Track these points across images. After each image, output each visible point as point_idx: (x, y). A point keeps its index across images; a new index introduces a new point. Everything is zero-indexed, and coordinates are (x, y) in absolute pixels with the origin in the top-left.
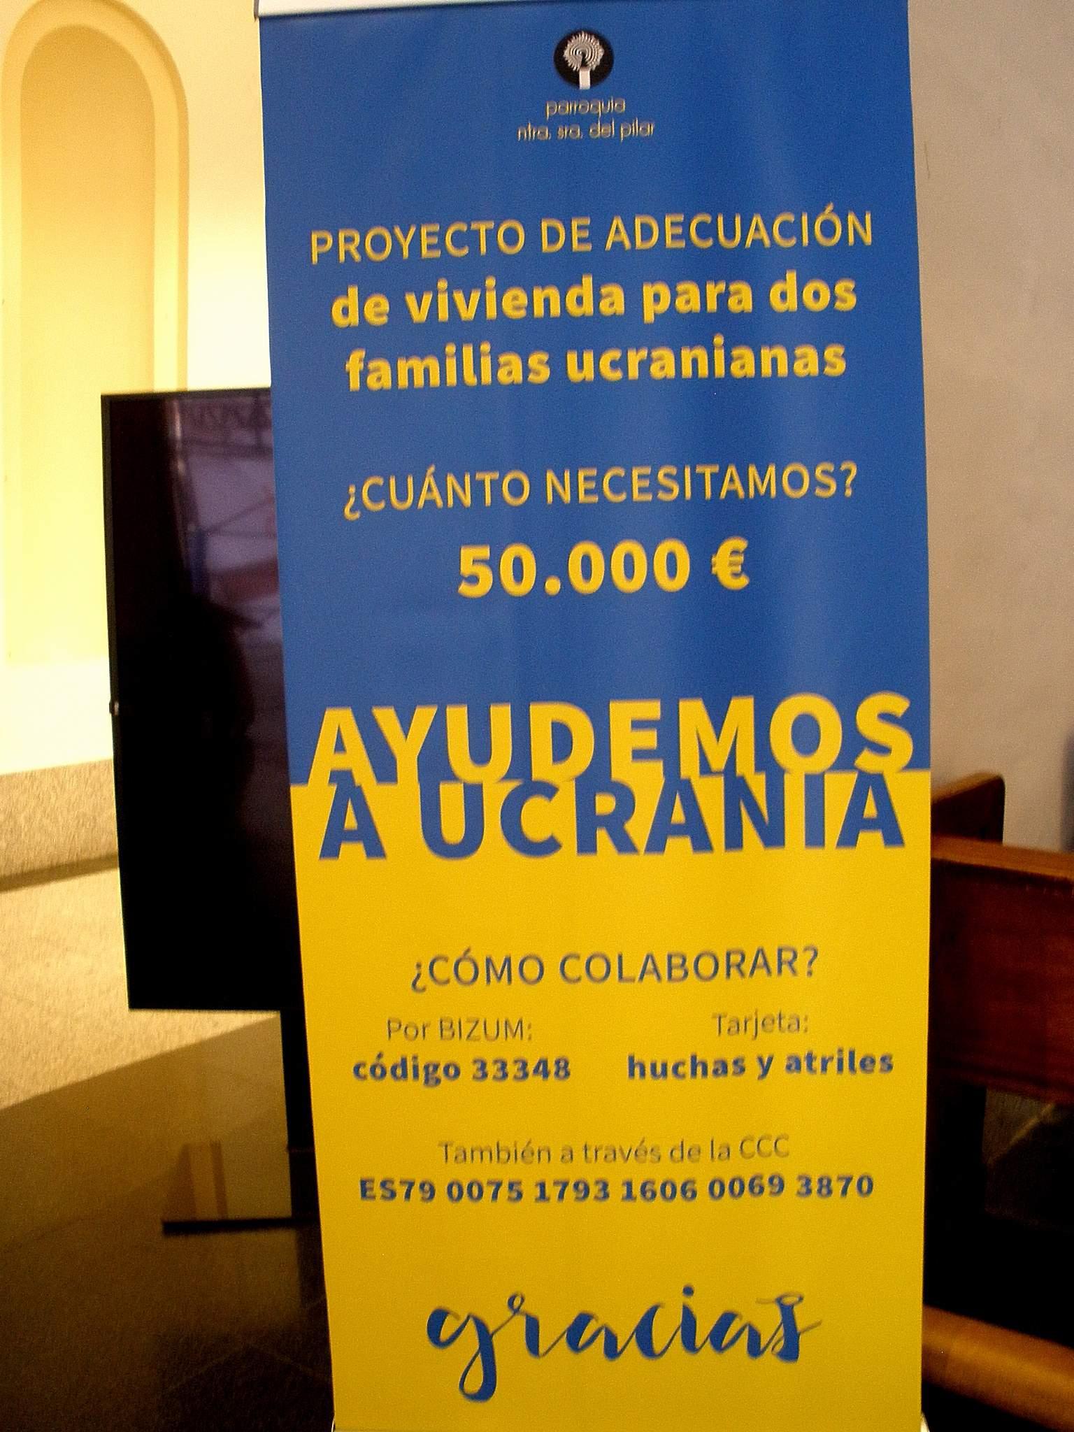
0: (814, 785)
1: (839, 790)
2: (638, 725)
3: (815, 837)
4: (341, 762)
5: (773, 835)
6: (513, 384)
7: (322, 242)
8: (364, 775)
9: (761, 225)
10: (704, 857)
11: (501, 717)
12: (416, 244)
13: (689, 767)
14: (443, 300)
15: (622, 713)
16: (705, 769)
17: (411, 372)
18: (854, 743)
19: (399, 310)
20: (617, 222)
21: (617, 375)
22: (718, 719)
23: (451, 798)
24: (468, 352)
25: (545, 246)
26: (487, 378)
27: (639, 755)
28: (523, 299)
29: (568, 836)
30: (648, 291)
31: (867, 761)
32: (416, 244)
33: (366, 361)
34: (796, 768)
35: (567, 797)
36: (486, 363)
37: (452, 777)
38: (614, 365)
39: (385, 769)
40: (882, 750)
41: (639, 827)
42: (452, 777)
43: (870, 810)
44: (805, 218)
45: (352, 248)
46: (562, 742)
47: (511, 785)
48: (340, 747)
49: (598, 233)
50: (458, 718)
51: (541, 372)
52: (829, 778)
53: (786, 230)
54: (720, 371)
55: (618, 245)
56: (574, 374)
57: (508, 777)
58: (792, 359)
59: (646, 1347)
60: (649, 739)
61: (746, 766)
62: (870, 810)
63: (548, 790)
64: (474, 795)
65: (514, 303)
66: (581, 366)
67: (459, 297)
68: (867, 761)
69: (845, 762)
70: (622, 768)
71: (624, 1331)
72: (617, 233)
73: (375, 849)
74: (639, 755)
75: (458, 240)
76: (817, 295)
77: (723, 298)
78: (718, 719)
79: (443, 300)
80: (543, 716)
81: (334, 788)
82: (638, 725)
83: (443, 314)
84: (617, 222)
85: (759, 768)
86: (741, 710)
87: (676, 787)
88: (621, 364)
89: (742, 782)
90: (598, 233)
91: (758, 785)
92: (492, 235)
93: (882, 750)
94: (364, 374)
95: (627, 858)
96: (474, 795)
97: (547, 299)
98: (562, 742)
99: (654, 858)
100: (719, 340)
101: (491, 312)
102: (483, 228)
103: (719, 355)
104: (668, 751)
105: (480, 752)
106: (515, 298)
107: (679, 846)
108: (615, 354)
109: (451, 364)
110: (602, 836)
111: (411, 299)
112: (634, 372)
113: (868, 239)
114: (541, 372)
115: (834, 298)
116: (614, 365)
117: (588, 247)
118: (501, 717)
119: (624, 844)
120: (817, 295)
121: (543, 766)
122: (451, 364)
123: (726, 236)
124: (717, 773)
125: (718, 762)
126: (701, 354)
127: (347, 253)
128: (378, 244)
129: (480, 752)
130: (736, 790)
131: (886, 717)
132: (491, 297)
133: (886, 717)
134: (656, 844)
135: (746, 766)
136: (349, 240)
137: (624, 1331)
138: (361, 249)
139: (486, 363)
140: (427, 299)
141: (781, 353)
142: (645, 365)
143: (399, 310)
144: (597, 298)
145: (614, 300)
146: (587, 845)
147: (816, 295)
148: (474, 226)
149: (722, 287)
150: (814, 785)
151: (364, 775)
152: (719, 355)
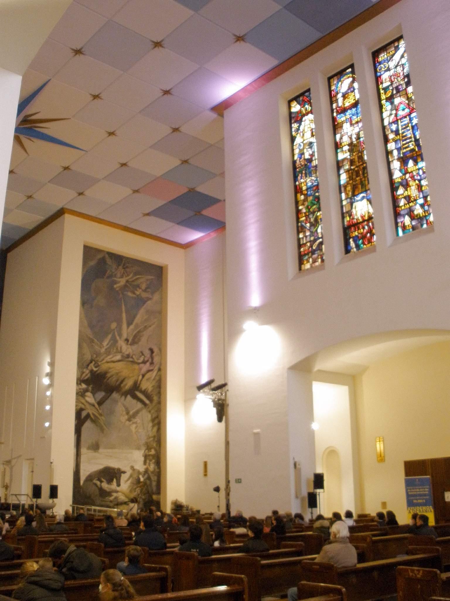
1: (429, 510)
70: (420, 509)
87: (423, 510)
130: (425, 510)
150: (428, 510)
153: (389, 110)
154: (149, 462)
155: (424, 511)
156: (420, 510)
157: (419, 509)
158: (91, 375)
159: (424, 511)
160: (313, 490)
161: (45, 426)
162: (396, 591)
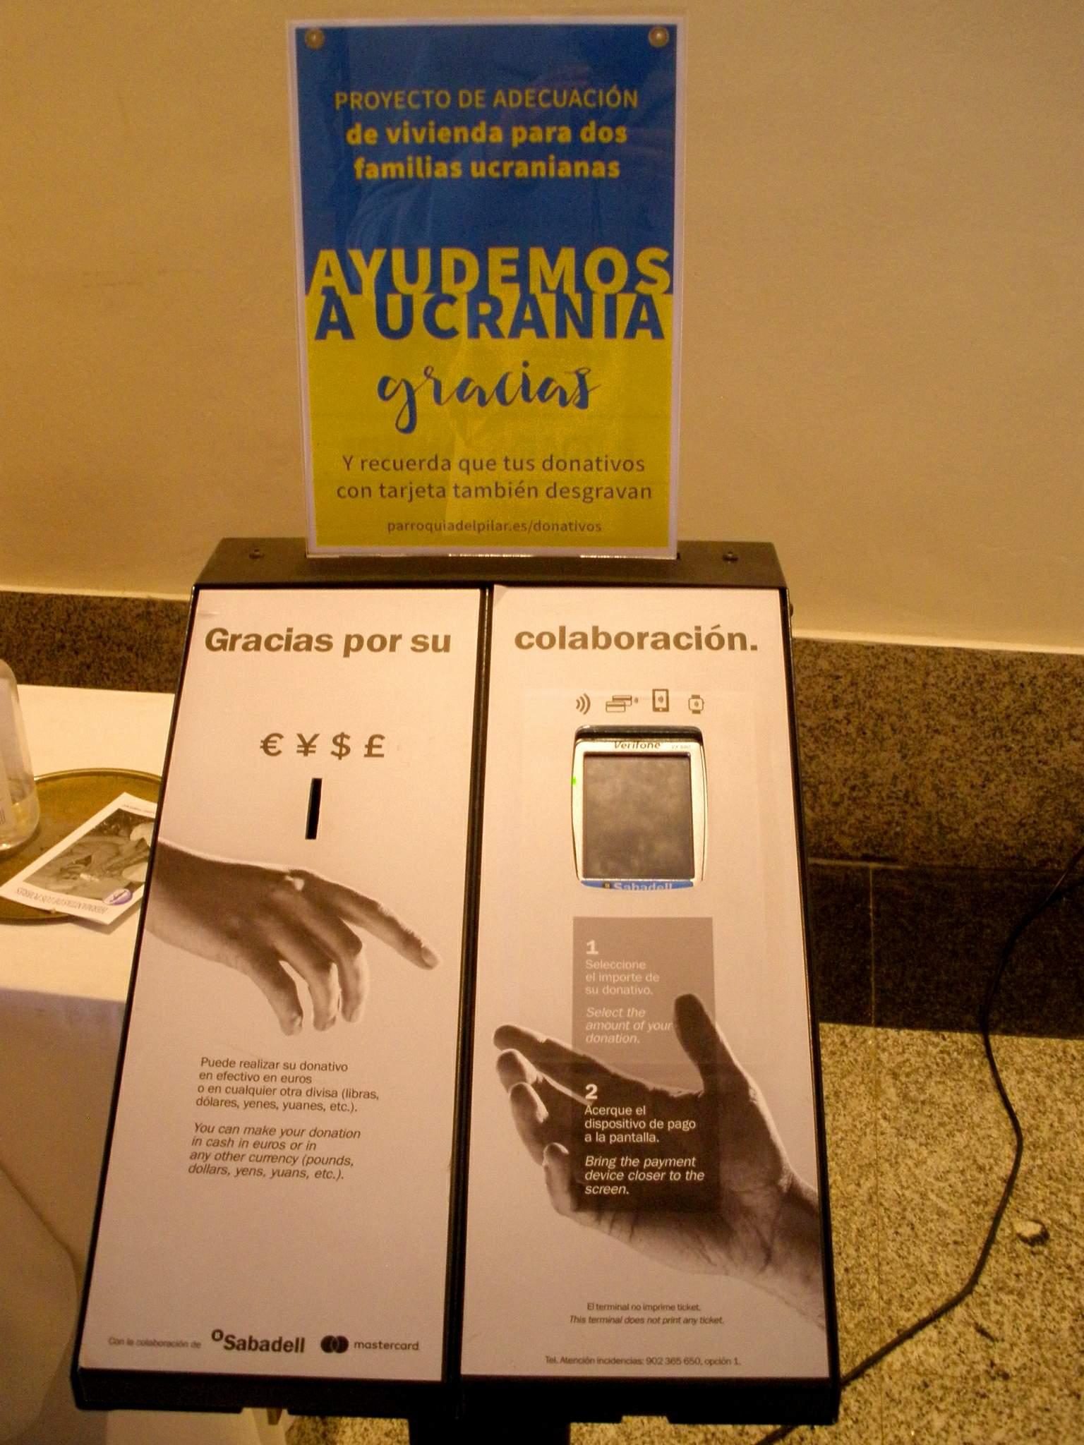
0: (611, 301)
1: (626, 304)
2: (506, 262)
3: (611, 332)
4: (329, 282)
5: (585, 330)
6: (442, 178)
7: (341, 98)
8: (342, 290)
9: (577, 95)
10: (544, 341)
11: (424, 256)
12: (392, 101)
13: (535, 287)
14: (406, 132)
15: (496, 255)
16: (545, 289)
17: (389, 171)
18: (635, 276)
19: (383, 137)
20: (500, 93)
21: (497, 175)
22: (553, 259)
23: (394, 302)
24: (419, 160)
25: (461, 105)
26: (429, 174)
27: (506, 280)
28: (449, 133)
29: (464, 329)
30: (515, 131)
31: (642, 287)
32: (392, 101)
33: (365, 163)
34: (600, 291)
35: (463, 302)
36: (429, 166)
37: (395, 291)
38: (496, 169)
39: (355, 288)
40: (652, 281)
41: (505, 323)
42: (395, 291)
43: (644, 316)
44: (601, 93)
45: (358, 102)
46: (460, 274)
47: (429, 296)
48: (328, 273)
49: (490, 97)
50: (398, 257)
51: (457, 173)
52: (620, 298)
53: (591, 98)
54: (552, 174)
55: (500, 105)
56: (475, 174)
57: (428, 291)
58: (591, 167)
59: (503, 401)
60: (512, 270)
61: (569, 288)
62: (644, 316)
63: (451, 300)
64: (407, 302)
65: (444, 135)
66: (478, 170)
67: (415, 131)
68: (642, 287)
69: (629, 288)
70: (495, 288)
71: (489, 389)
72: (499, 98)
73: (348, 334)
74: (506, 280)
75: (415, 100)
76: (606, 134)
77: (555, 135)
78: (553, 259)
79: (406, 132)
80: (449, 256)
81: (323, 298)
82: (506, 262)
83: (407, 139)
84: (500, 93)
85: (577, 290)
86: (567, 257)
87: (527, 299)
88: (499, 169)
89: (567, 297)
90: (490, 97)
91: (577, 300)
92: (433, 97)
93: (652, 281)
94: (364, 170)
95: (498, 341)
96: (407, 302)
97: (461, 134)
98: (460, 274)
99: (513, 341)
100: (552, 157)
101: (432, 140)
102: (428, 93)
103: (552, 165)
104: (522, 277)
105: (412, 276)
106: (445, 132)
107: (528, 334)
108: (496, 164)
109: (410, 166)
110: (483, 328)
111: (389, 131)
112: (506, 173)
113: (635, 104)
114: (457, 173)
115: (615, 136)
116: (496, 169)
117: (483, 106)
118: (424, 256)
119: (496, 333)
120: (606, 134)
121: (448, 286)
122: (410, 166)
123: (558, 99)
124: (551, 292)
125: (552, 285)
126: (542, 165)
127: (356, 106)
128: (372, 101)
129: (412, 276)
130: (563, 302)
131: (655, 262)
132: (432, 131)
133: (655, 262)
134: (515, 333)
135: (569, 288)
136: (356, 97)
137: (489, 389)
138: (363, 102)
139: (429, 166)
140: (398, 131)
141: (585, 165)
142: (512, 170)
143: (383, 137)
144: (488, 133)
145: (497, 136)
146: (474, 333)
147: (606, 135)
148: (423, 92)
149: (554, 129)
150: (611, 301)
151: (342, 290)
152: (552, 165)
153: (1005, 1383)
154: (1006, 1386)
155: (548, 305)
156: (480, 293)
157: (470, 282)
158: (979, 1033)
159: (548, 305)
160: (437, 377)
161: (329, 248)
162: (693, 877)
